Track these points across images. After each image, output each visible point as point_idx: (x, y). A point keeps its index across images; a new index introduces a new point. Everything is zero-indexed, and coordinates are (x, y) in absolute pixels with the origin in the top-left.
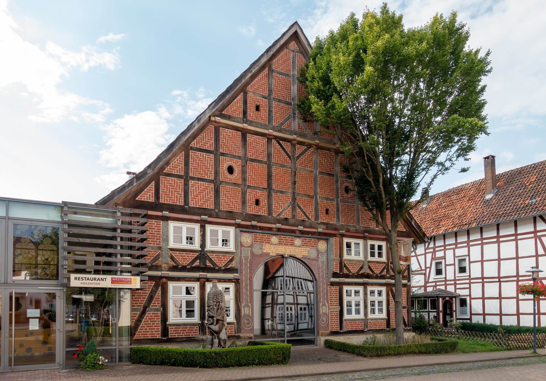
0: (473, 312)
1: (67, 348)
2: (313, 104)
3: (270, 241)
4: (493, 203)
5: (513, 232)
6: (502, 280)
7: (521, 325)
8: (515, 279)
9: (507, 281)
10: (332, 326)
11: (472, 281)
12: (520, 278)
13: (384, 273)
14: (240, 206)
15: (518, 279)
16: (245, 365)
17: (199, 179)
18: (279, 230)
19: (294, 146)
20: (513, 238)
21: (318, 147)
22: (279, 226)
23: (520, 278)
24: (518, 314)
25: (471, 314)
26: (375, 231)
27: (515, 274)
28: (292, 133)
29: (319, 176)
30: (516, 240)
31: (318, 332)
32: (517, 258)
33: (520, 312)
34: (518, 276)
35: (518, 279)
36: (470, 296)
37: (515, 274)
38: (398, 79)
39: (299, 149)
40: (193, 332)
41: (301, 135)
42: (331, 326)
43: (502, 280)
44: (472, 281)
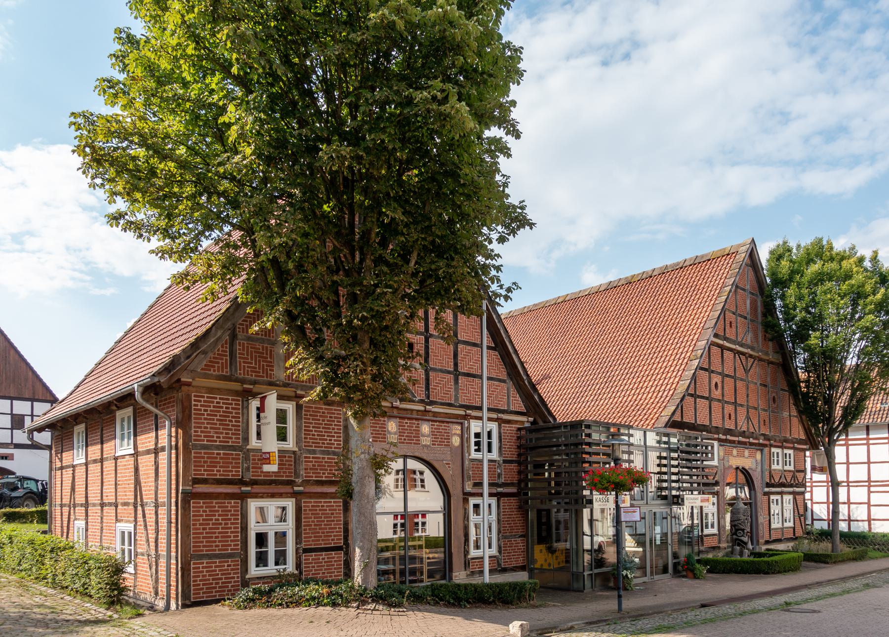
0: (814, 518)
1: (267, 551)
2: (306, 235)
3: (385, 428)
4: (878, 409)
5: (865, 436)
6: (850, 484)
7: (852, 530)
8: (867, 484)
9: (857, 486)
10: (235, 519)
11: (814, 484)
12: (872, 484)
13: (792, 482)
14: (422, 391)
15: (869, 484)
16: (779, 572)
17: (441, 371)
18: (740, 442)
19: (747, 358)
20: (865, 442)
21: (760, 360)
22: (741, 439)
23: (872, 484)
24: (869, 520)
25: (813, 520)
26: (789, 440)
27: (866, 479)
28: (748, 347)
29: (760, 387)
30: (868, 445)
31: (758, 541)
32: (869, 463)
33: (872, 518)
34: (869, 481)
35: (869, 484)
36: (811, 500)
37: (866, 479)
38: (416, 199)
39: (751, 360)
40: (335, 536)
41: (753, 349)
42: (238, 519)
43: (850, 484)
44: (814, 484)
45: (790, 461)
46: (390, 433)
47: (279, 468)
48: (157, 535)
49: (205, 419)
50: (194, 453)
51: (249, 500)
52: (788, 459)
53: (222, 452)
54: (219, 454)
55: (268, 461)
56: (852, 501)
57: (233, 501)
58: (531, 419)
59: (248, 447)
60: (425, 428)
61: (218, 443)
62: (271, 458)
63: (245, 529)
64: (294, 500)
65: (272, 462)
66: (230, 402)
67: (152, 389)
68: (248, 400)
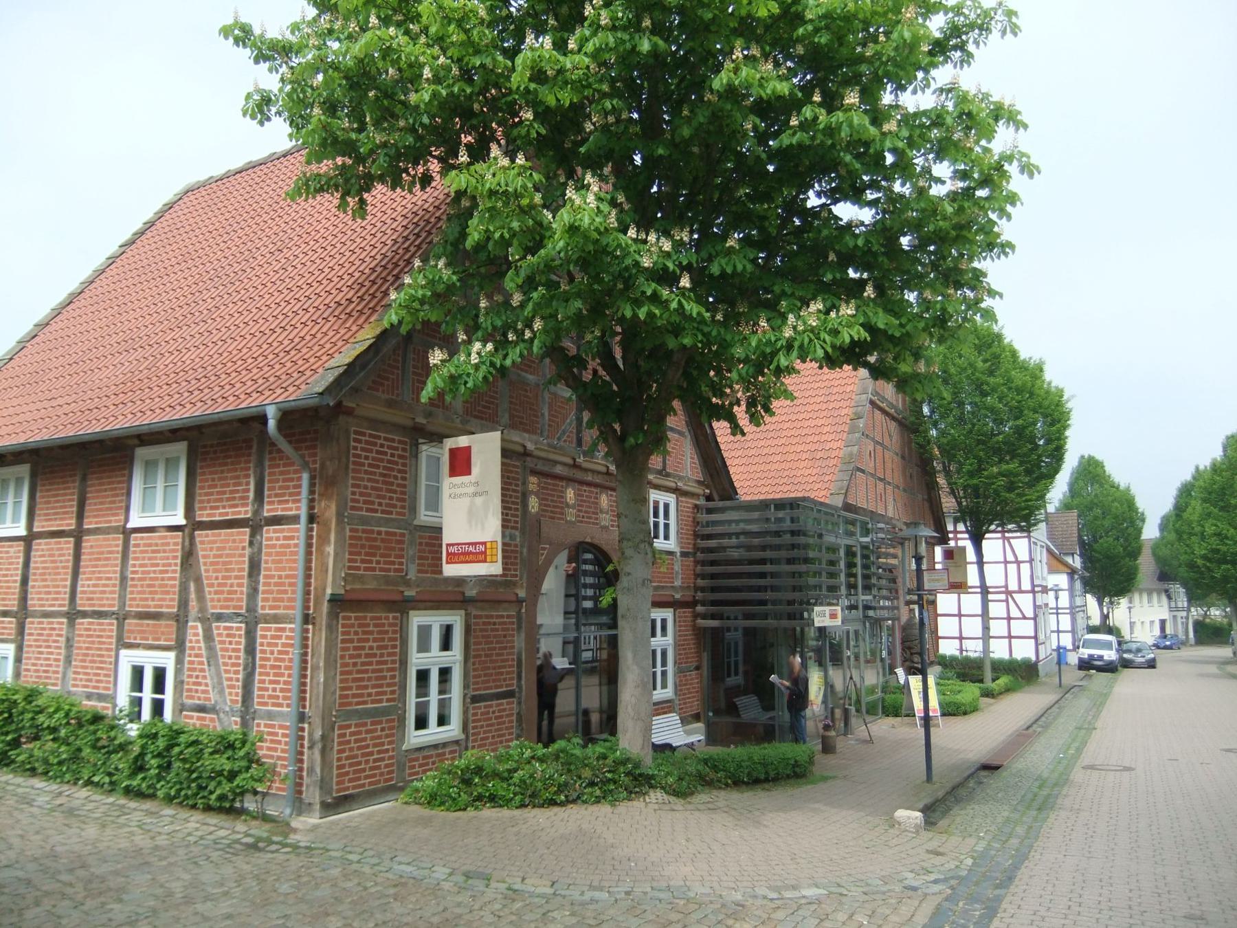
45: (667, 526)
46: (568, 506)
47: (504, 569)
48: (122, 572)
49: (366, 472)
50: (351, 530)
51: (411, 612)
52: (661, 520)
53: (383, 529)
54: (379, 533)
55: (481, 557)
56: (1005, 622)
57: (391, 615)
58: (708, 491)
59: (416, 522)
60: (570, 494)
61: (379, 515)
62: (488, 552)
63: (404, 663)
64: (463, 612)
65: (489, 559)
66: (395, 445)
67: (292, 418)
68: (417, 445)
